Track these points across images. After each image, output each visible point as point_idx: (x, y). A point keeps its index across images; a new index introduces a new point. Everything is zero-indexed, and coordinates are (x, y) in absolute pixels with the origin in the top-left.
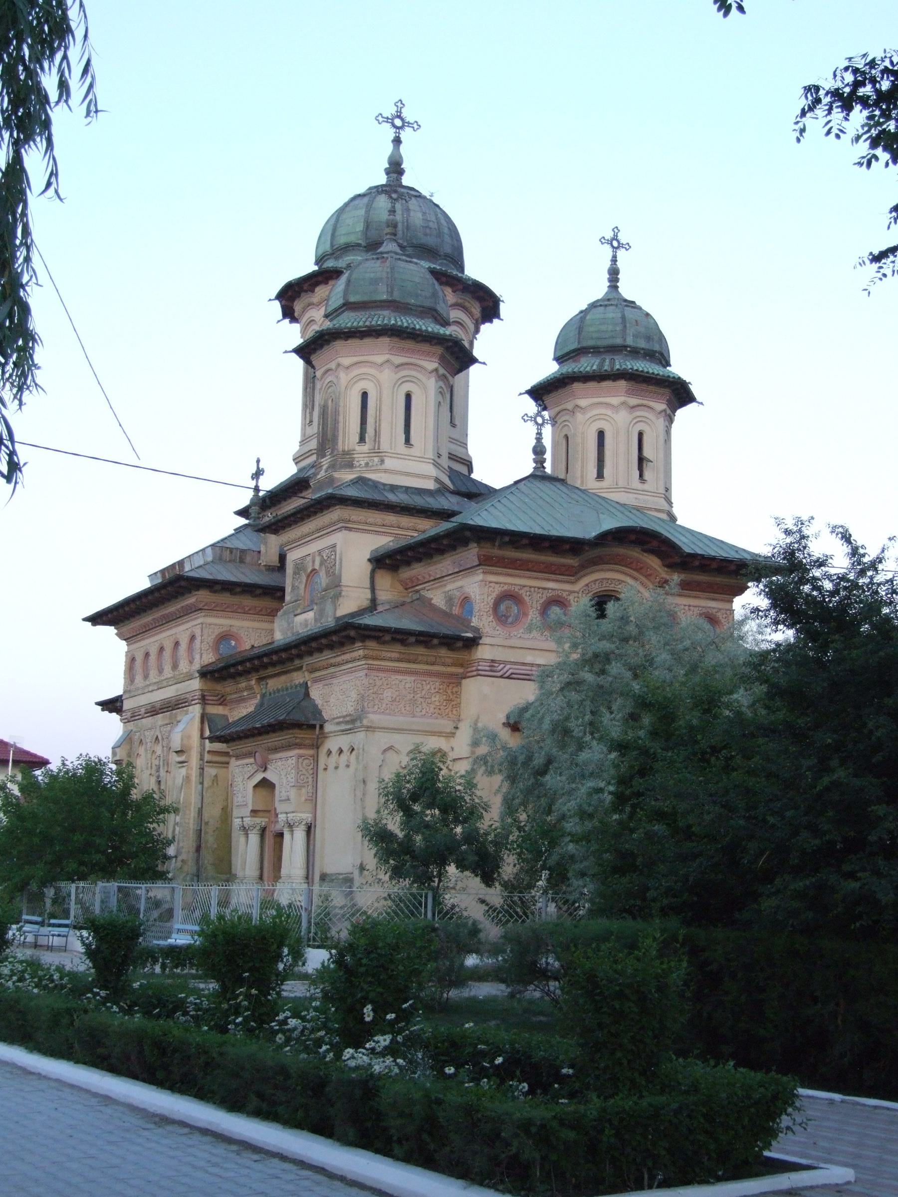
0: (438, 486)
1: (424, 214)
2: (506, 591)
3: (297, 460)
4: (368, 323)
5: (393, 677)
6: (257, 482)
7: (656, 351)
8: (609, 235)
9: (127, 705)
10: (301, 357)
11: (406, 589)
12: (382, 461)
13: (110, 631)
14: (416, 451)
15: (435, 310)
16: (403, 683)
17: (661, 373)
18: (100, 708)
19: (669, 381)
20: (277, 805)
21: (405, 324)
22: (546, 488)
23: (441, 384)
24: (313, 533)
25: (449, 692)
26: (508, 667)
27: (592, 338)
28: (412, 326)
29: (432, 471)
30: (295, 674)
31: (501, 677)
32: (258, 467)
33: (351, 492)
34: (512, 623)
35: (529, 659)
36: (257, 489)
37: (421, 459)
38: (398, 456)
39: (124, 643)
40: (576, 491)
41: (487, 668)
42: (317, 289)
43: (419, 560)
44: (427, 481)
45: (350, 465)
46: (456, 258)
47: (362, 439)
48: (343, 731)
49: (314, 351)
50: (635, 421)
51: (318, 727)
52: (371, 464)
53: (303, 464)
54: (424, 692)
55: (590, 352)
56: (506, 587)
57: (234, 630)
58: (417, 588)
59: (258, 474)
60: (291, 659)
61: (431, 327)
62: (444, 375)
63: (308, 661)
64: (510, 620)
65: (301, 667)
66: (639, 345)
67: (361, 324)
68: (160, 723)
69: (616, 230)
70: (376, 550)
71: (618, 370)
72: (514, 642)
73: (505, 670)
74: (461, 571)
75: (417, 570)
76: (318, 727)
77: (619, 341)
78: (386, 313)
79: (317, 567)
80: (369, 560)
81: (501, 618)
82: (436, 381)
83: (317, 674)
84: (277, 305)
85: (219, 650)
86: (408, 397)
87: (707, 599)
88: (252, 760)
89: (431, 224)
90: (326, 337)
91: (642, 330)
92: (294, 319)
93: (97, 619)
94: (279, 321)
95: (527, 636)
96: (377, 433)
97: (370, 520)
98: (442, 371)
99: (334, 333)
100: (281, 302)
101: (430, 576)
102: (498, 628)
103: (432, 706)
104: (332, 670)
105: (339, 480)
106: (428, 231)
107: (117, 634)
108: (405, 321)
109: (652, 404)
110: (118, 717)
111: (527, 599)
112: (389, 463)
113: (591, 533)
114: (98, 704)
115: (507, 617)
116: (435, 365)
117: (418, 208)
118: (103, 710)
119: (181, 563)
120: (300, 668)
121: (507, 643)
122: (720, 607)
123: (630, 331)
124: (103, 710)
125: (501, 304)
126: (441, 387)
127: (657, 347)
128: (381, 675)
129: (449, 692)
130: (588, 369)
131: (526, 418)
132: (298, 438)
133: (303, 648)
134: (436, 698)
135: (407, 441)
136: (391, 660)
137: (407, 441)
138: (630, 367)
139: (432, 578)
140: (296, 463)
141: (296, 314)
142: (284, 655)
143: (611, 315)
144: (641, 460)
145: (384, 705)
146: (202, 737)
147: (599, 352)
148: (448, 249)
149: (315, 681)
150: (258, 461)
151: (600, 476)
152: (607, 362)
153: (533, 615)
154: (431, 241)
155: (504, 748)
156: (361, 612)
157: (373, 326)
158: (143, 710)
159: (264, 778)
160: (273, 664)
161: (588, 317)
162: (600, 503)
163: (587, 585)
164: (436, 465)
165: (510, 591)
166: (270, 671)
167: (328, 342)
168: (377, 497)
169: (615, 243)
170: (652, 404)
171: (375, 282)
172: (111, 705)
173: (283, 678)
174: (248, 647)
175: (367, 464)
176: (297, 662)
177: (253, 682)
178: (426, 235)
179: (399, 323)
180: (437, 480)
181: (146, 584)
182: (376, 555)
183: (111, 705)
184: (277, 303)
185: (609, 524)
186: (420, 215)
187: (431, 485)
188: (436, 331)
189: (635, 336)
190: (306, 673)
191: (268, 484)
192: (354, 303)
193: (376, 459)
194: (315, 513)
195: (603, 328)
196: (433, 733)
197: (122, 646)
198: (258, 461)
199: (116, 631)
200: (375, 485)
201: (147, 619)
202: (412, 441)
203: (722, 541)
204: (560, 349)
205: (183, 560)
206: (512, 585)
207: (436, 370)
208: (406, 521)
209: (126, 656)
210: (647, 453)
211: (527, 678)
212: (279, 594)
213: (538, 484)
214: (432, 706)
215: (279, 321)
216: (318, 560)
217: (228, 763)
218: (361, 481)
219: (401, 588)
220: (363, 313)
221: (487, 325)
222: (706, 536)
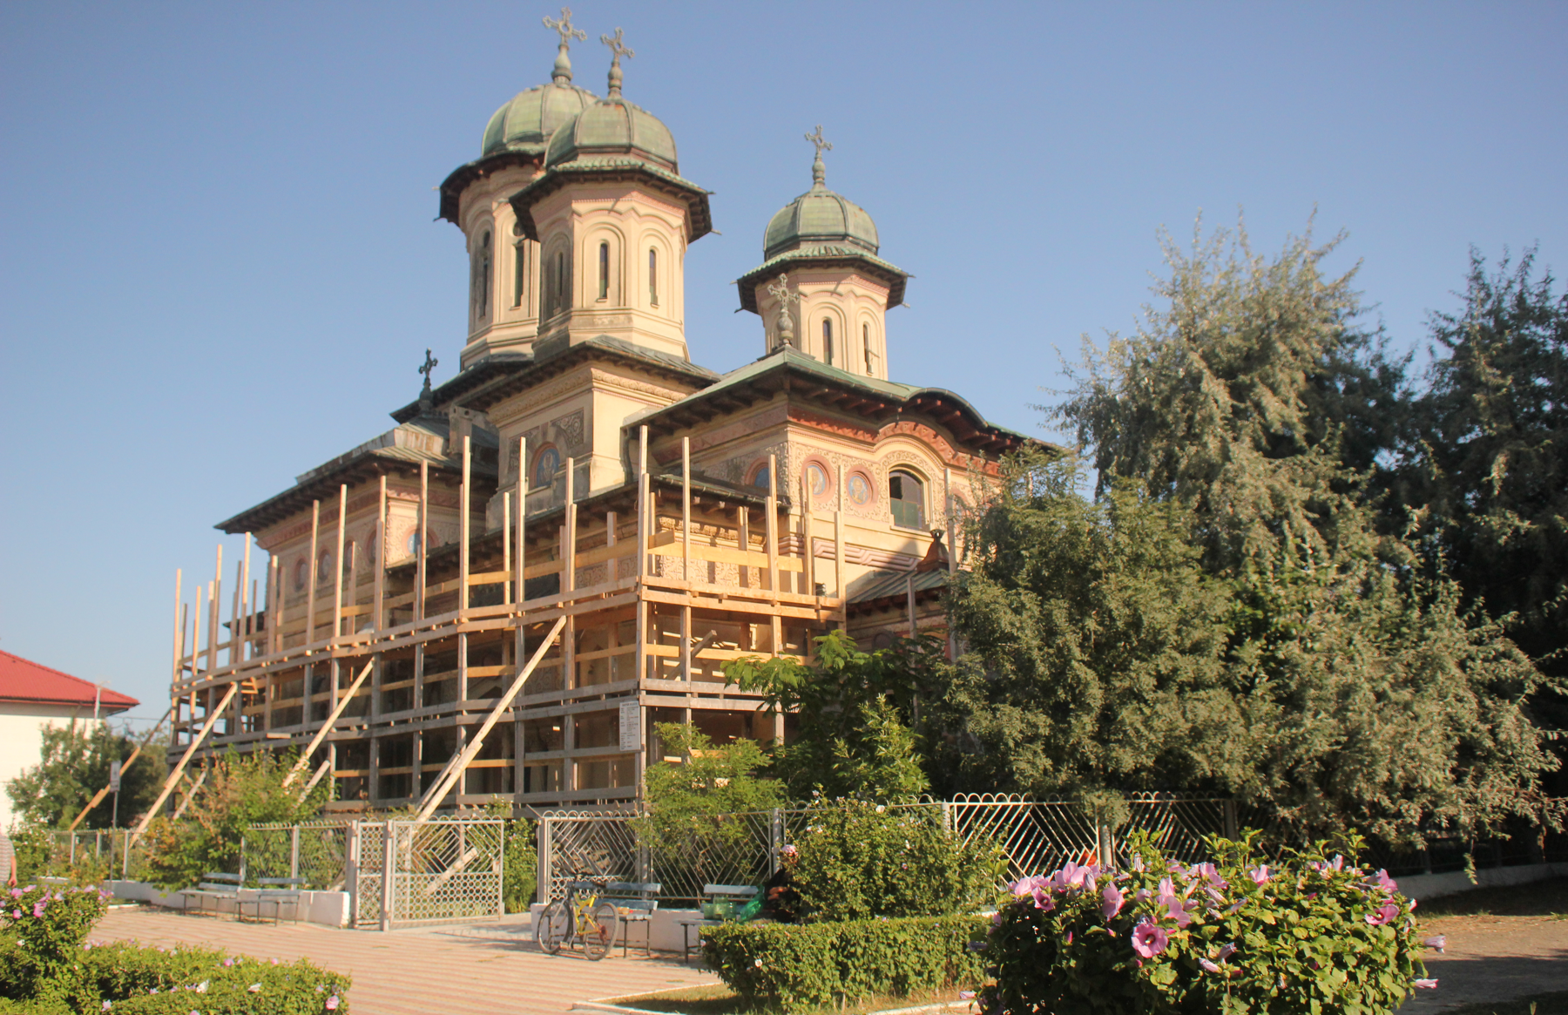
12: (630, 320)
14: (662, 311)
59: (430, 364)
77: (841, 230)
93: (234, 526)
112: (637, 322)
127: (874, 242)
135: (654, 301)
170: (875, 296)
171: (612, 125)
189: (856, 227)
198: (428, 353)
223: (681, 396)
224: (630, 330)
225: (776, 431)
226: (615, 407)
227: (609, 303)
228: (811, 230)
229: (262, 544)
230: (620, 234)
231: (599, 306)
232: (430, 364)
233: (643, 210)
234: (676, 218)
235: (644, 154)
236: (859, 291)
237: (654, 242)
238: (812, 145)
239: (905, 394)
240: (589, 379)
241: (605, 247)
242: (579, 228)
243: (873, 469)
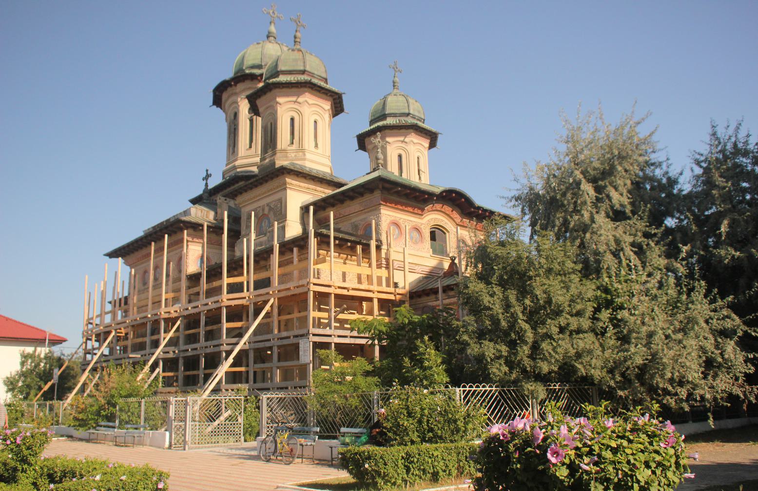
12: (305, 155)
14: (320, 151)
36: (207, 185)
42: (238, 85)
56: (393, 218)
59: (208, 176)
77: (406, 111)
93: (113, 254)
96: (301, 140)
127: (423, 117)
132: (225, 162)
135: (316, 146)
137: (316, 146)
144: (419, 171)
150: (207, 171)
167: (270, 90)
171: (296, 60)
174: (213, 263)
181: (141, 234)
189: (414, 110)
191: (213, 183)
193: (301, 153)
198: (207, 171)
202: (319, 146)
210: (422, 168)
216: (267, 209)
224: (305, 159)
225: (376, 208)
226: (297, 197)
227: (294, 147)
228: (392, 111)
229: (127, 263)
230: (300, 113)
231: (289, 148)
232: (208, 176)
233: (311, 102)
236: (415, 141)
240: (285, 183)
241: (292, 120)
243: (422, 227)
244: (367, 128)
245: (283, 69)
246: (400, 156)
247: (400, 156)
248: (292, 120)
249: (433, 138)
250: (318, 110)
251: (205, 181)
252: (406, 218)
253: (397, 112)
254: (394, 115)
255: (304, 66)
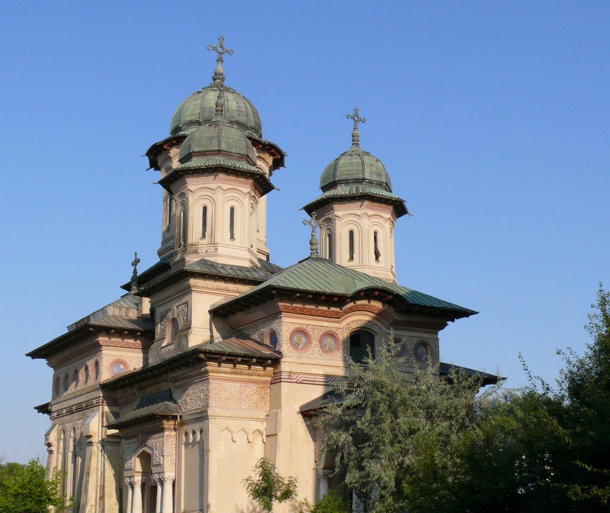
0: (251, 265)
1: (238, 103)
2: (298, 328)
3: (160, 253)
4: (207, 164)
5: (227, 384)
6: (135, 267)
7: (383, 183)
8: (352, 113)
9: (54, 408)
10: (164, 187)
11: (232, 329)
12: (216, 249)
13: (44, 361)
14: (237, 242)
15: (248, 156)
16: (233, 388)
17: (387, 195)
18: (37, 410)
19: (392, 200)
20: (152, 468)
21: (230, 164)
22: (320, 266)
23: (252, 201)
24: (173, 295)
25: (263, 392)
26: (300, 376)
27: (344, 175)
28: (234, 165)
29: (249, 256)
30: (163, 384)
31: (296, 382)
32: (136, 258)
33: (198, 269)
34: (301, 348)
35: (313, 371)
37: (241, 248)
38: (227, 246)
39: (52, 369)
40: (338, 267)
41: (287, 377)
43: (241, 310)
44: (245, 261)
45: (196, 252)
46: (257, 129)
47: (204, 236)
48: (195, 419)
49: (172, 182)
50: (372, 224)
51: (179, 417)
52: (209, 251)
53: (164, 256)
54: (247, 393)
55: (343, 183)
57: (122, 358)
58: (240, 328)
59: (136, 262)
60: (160, 375)
61: (244, 166)
62: (253, 196)
63: (172, 375)
64: (300, 346)
65: (167, 379)
66: (373, 179)
67: (202, 164)
68: (76, 418)
69: (356, 110)
70: (213, 305)
71: (361, 193)
72: (304, 360)
73: (298, 378)
74: (268, 316)
75: (239, 317)
76: (179, 417)
77: (361, 176)
78: (217, 158)
79: (175, 317)
80: (209, 311)
81: (295, 346)
82: (249, 200)
83: (177, 384)
84: (147, 159)
85: (113, 371)
86: (232, 209)
87: (422, 332)
88: (135, 440)
89: (242, 109)
90: (181, 173)
91: (374, 169)
92: (157, 168)
93: (35, 354)
94: (148, 169)
95: (311, 357)
97: (210, 286)
98: (253, 194)
99: (185, 170)
100: (149, 157)
101: (248, 320)
102: (293, 351)
103: (252, 402)
104: (188, 380)
105: (189, 261)
106: (240, 113)
107: (47, 364)
108: (229, 163)
109: (382, 214)
110: (49, 416)
111: (311, 333)
112: (221, 250)
113: (351, 291)
114: (36, 408)
115: (299, 345)
116: (249, 190)
117: (234, 100)
118: (39, 412)
119: (88, 318)
120: (166, 380)
121: (299, 361)
122: (431, 337)
123: (367, 170)
124: (39, 412)
125: (285, 157)
126: (252, 204)
127: (384, 180)
128: (219, 382)
129: (263, 392)
130: (343, 193)
131: (305, 222)
133: (168, 367)
134: (256, 396)
135: (232, 237)
136: (225, 373)
137: (232, 237)
138: (368, 191)
139: (250, 321)
140: (159, 256)
141: (159, 164)
142: (156, 372)
143: (355, 161)
145: (221, 402)
146: (102, 426)
147: (349, 183)
148: (253, 124)
149: (176, 388)
151: (352, 258)
152: (354, 189)
153: (315, 343)
154: (242, 119)
155: (160, 462)
156: (205, 344)
157: (209, 165)
158: (65, 411)
159: (144, 451)
160: (149, 378)
161: (341, 162)
162: (353, 274)
163: (348, 324)
164: (250, 251)
165: (300, 328)
166: (147, 382)
168: (214, 272)
169: (356, 118)
170: (382, 214)
171: (210, 139)
172: (44, 409)
173: (155, 387)
175: (207, 251)
176: (164, 376)
177: (136, 391)
178: (239, 115)
179: (226, 164)
180: (251, 261)
181: (66, 331)
182: (213, 308)
183: (44, 409)
184: (147, 157)
185: (360, 286)
186: (235, 103)
187: (247, 264)
188: (249, 168)
189: (371, 173)
190: (170, 383)
191: (142, 269)
192: (198, 152)
194: (170, 285)
195: (351, 168)
196: (253, 419)
197: (51, 371)
198: (136, 254)
199: (47, 362)
200: (213, 265)
201: (66, 353)
202: (235, 237)
203: (430, 296)
204: (324, 182)
205: (89, 316)
206: (301, 324)
207: (249, 193)
208: (231, 286)
209: (53, 377)
211: (313, 383)
212: (150, 335)
213: (314, 264)
214: (252, 402)
215: (148, 169)
217: (120, 443)
218: (203, 262)
219: (229, 328)
220: (203, 158)
221: (277, 170)
222: (420, 293)
223: (246, 290)
224: (216, 255)
225: (276, 315)
226: (203, 300)
227: (206, 241)
228: (343, 178)
229: (50, 364)
230: (214, 201)
231: (200, 241)
232: (136, 262)
233: (225, 187)
234: (246, 187)
235: (227, 154)
236: (371, 213)
237: (233, 203)
238: (352, 121)
239: (251, 341)
240: (189, 287)
241: (205, 209)
242: (191, 198)
243: (338, 332)
244: (319, 195)
245: (196, 150)
246: (351, 233)
247: (351, 233)
248: (205, 209)
249: (399, 209)
250: (238, 196)
251: (133, 268)
252: (316, 325)
253: (349, 177)
254: (347, 182)
255: (219, 145)
